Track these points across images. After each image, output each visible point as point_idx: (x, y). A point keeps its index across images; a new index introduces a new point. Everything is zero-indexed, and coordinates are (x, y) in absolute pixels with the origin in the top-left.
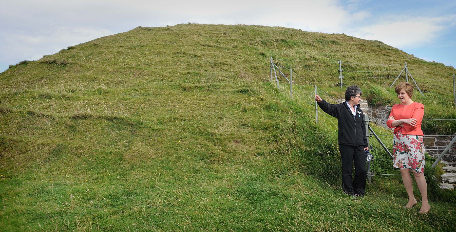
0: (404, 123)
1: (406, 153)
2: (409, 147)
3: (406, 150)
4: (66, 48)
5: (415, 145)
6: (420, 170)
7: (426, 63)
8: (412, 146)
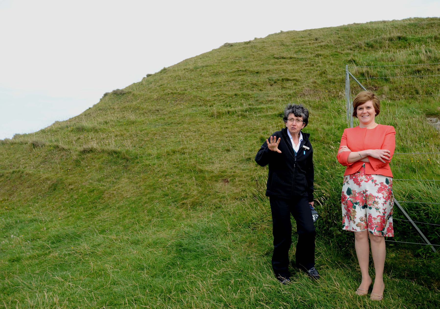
0: (369, 157)
2: (375, 197)
8: (380, 195)
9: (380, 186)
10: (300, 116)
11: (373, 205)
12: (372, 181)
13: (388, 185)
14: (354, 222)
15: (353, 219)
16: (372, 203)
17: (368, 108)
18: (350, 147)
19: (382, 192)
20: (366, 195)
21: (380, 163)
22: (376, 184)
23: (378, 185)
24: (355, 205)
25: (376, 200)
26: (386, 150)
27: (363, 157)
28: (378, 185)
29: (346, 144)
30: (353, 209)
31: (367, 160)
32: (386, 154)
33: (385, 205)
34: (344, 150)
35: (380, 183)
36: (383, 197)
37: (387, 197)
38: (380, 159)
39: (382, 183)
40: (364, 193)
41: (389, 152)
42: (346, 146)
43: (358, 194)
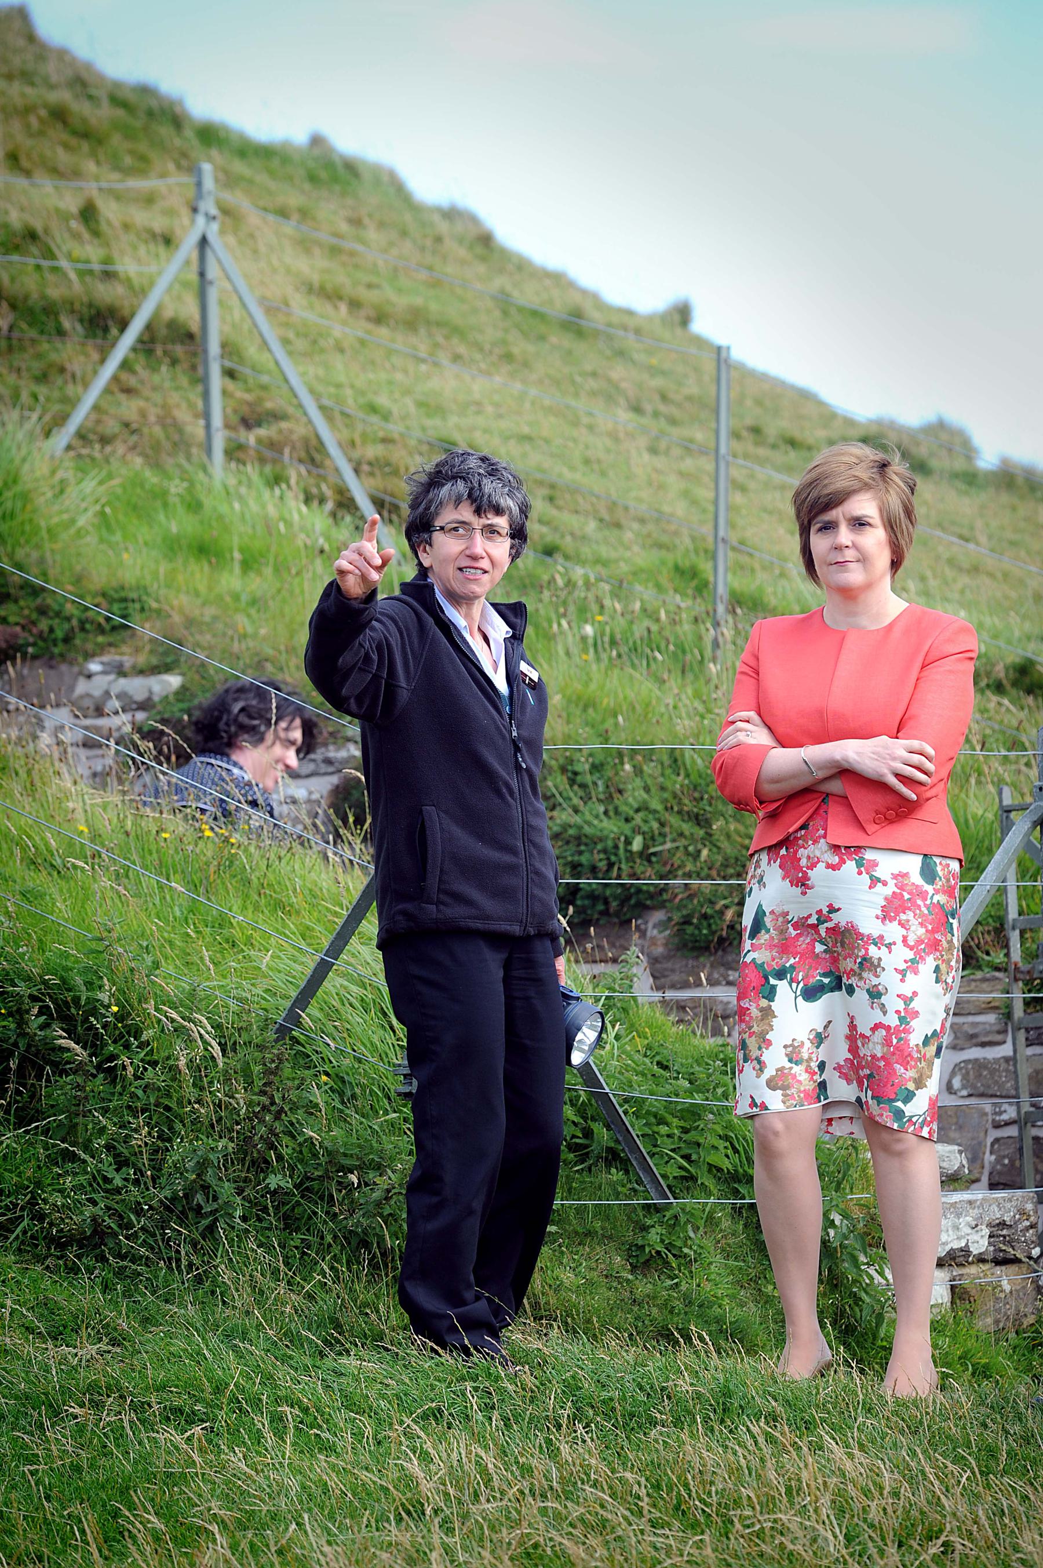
0: (845, 772)
1: (837, 985)
2: (870, 940)
3: (848, 964)
4: (988, 459)
5: (914, 924)
6: (918, 1106)
7: (248, 151)
8: (893, 931)
9: (891, 889)
10: (498, 511)
11: (861, 978)
12: (912, 961)
13: (929, 889)
14: (761, 1066)
15: (754, 1053)
16: (856, 967)
17: (859, 523)
18: (767, 720)
19: (903, 917)
20: (834, 931)
21: (890, 799)
22: (875, 881)
23: (885, 884)
24: (772, 981)
25: (873, 951)
26: (916, 744)
27: (821, 775)
28: (885, 884)
29: (754, 704)
30: (764, 1003)
31: (836, 786)
32: (916, 759)
33: (909, 975)
34: (741, 737)
35: (895, 877)
36: (905, 940)
37: (920, 941)
38: (892, 781)
39: (900, 877)
40: (822, 918)
41: (931, 751)
42: (752, 714)
43: (796, 926)
